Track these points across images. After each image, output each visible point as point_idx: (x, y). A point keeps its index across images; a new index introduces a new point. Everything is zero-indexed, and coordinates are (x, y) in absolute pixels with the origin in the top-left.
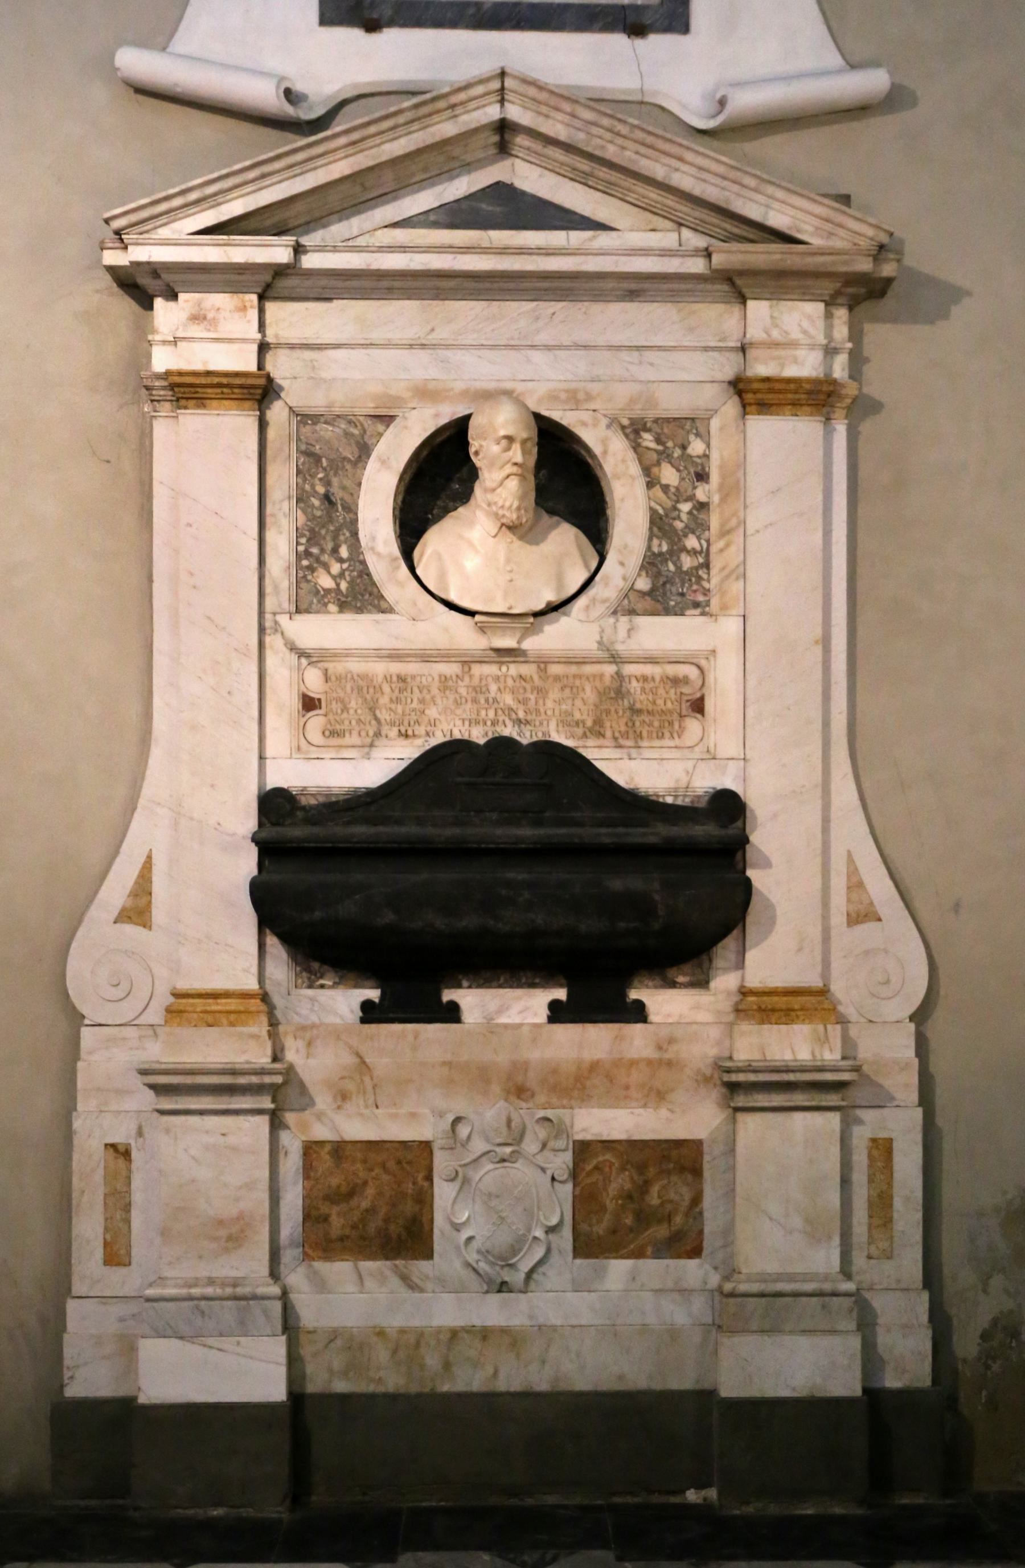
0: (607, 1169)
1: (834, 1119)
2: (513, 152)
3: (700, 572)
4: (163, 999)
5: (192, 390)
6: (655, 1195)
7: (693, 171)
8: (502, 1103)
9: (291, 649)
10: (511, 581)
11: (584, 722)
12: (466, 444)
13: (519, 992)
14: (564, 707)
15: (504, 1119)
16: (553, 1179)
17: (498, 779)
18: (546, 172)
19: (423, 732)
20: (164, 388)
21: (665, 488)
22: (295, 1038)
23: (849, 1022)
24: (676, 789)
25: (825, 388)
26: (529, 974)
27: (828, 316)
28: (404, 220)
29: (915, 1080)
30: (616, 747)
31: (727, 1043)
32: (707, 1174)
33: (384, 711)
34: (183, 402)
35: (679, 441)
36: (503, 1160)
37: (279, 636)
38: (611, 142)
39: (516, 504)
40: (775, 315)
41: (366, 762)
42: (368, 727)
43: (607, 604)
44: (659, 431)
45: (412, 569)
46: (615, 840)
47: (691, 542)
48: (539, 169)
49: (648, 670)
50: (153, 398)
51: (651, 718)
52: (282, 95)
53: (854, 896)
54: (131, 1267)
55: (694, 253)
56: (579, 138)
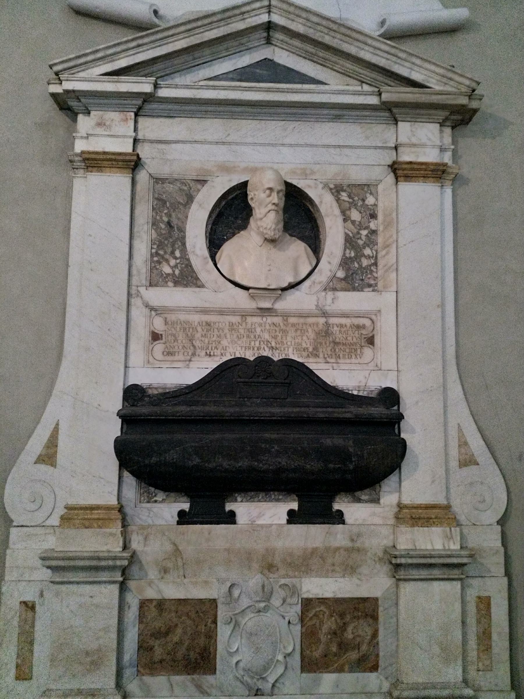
0: (321, 616)
1: (457, 585)
2: (274, 43)
3: (372, 268)
4: (60, 511)
5: (96, 162)
6: (350, 632)
7: (371, 50)
8: (259, 576)
9: (146, 306)
10: (270, 270)
11: (307, 348)
12: (246, 195)
13: (270, 504)
14: (297, 341)
15: (260, 585)
16: (289, 622)
17: (260, 380)
18: (291, 54)
19: (219, 354)
20: (80, 161)
21: (353, 222)
22: (138, 533)
23: (461, 525)
24: (359, 387)
25: (441, 168)
26: (276, 493)
27: (441, 131)
28: (215, 77)
29: (502, 560)
30: (326, 363)
31: (391, 537)
32: (381, 619)
33: (198, 342)
34: (90, 169)
35: (361, 197)
36: (259, 611)
37: (139, 299)
38: (327, 34)
39: (273, 227)
40: (414, 130)
41: (187, 370)
42: (189, 350)
43: (322, 285)
44: (350, 191)
45: (215, 265)
46: (327, 416)
47: (367, 251)
48: (288, 53)
49: (343, 321)
50: (73, 167)
51: (344, 347)
52: (152, 12)
53: (463, 451)
54: (32, 681)
55: (372, 93)
56: (310, 32)
